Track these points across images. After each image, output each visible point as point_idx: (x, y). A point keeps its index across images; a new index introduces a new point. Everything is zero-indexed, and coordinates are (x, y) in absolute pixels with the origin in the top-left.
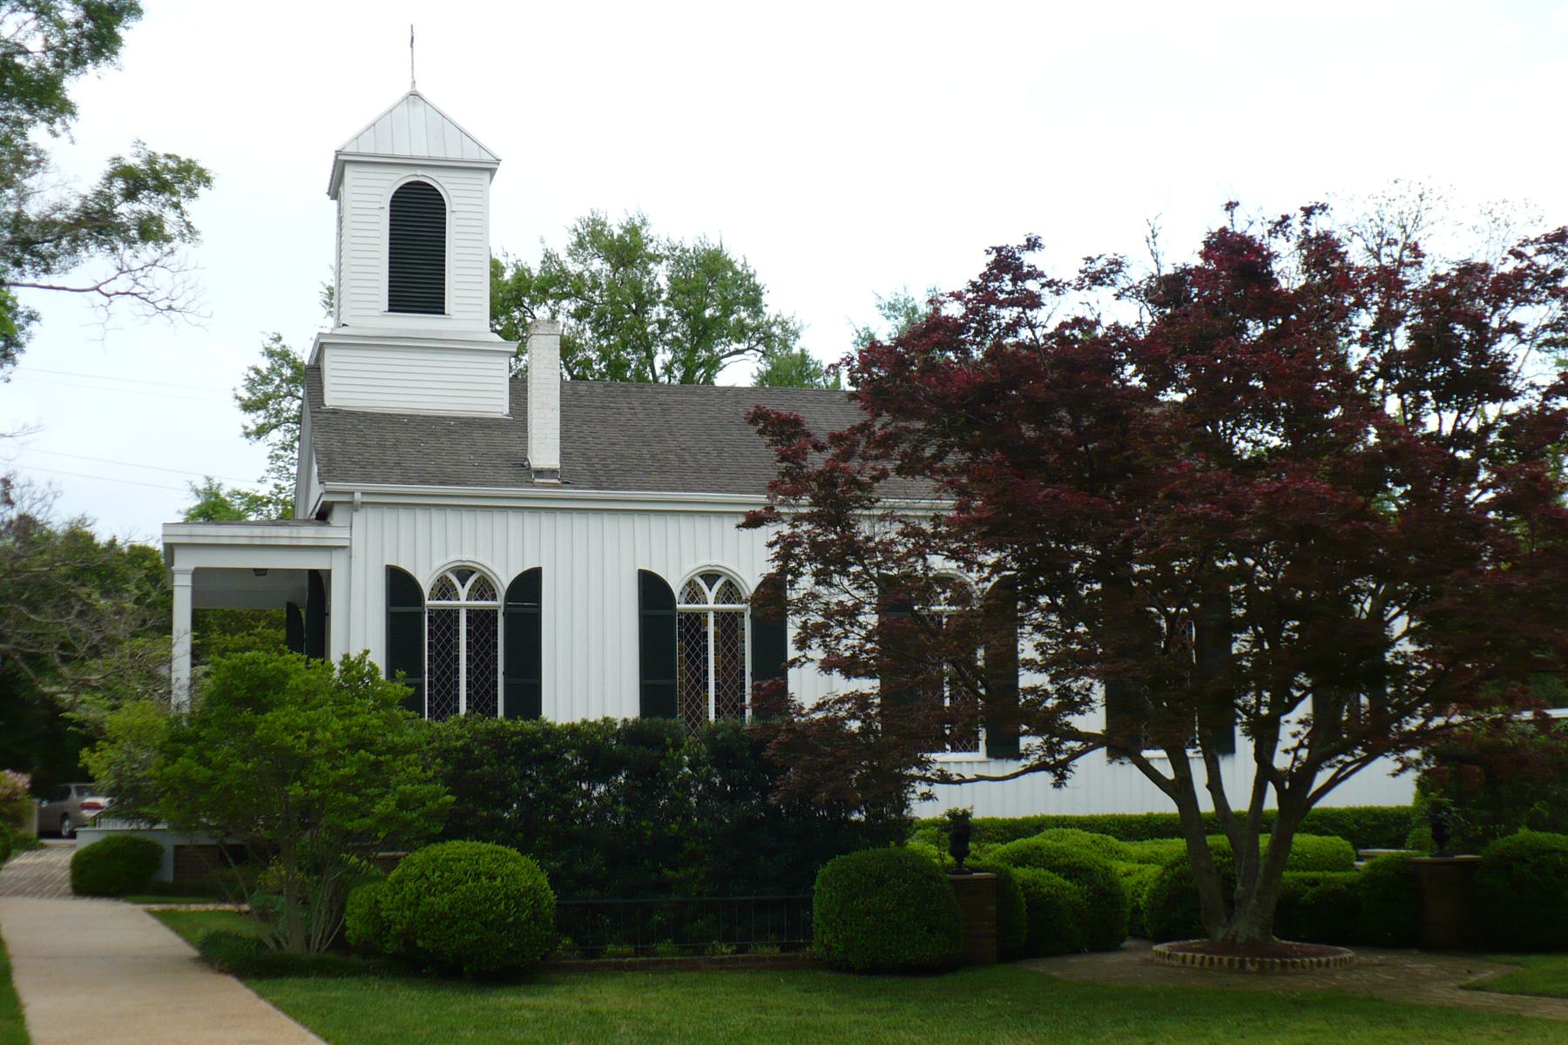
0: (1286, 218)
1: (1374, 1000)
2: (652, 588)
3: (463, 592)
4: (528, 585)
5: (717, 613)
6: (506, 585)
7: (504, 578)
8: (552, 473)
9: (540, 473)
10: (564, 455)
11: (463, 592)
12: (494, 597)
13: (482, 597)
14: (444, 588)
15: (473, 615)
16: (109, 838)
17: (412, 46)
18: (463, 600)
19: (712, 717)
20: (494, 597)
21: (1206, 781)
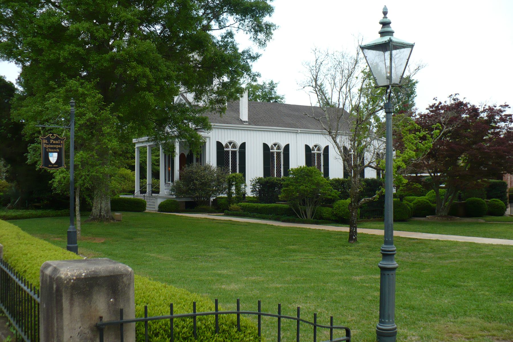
0: (452, 95)
1: (324, 96)
2: (266, 147)
3: (230, 147)
4: (243, 146)
5: (276, 152)
6: (239, 145)
7: (239, 144)
8: (246, 122)
9: (244, 122)
10: (249, 119)
11: (230, 147)
12: (236, 148)
13: (234, 148)
14: (227, 146)
15: (232, 152)
16: (168, 200)
17: (339, 98)
18: (230, 149)
19: (275, 176)
20: (236, 148)
21: (363, 232)
